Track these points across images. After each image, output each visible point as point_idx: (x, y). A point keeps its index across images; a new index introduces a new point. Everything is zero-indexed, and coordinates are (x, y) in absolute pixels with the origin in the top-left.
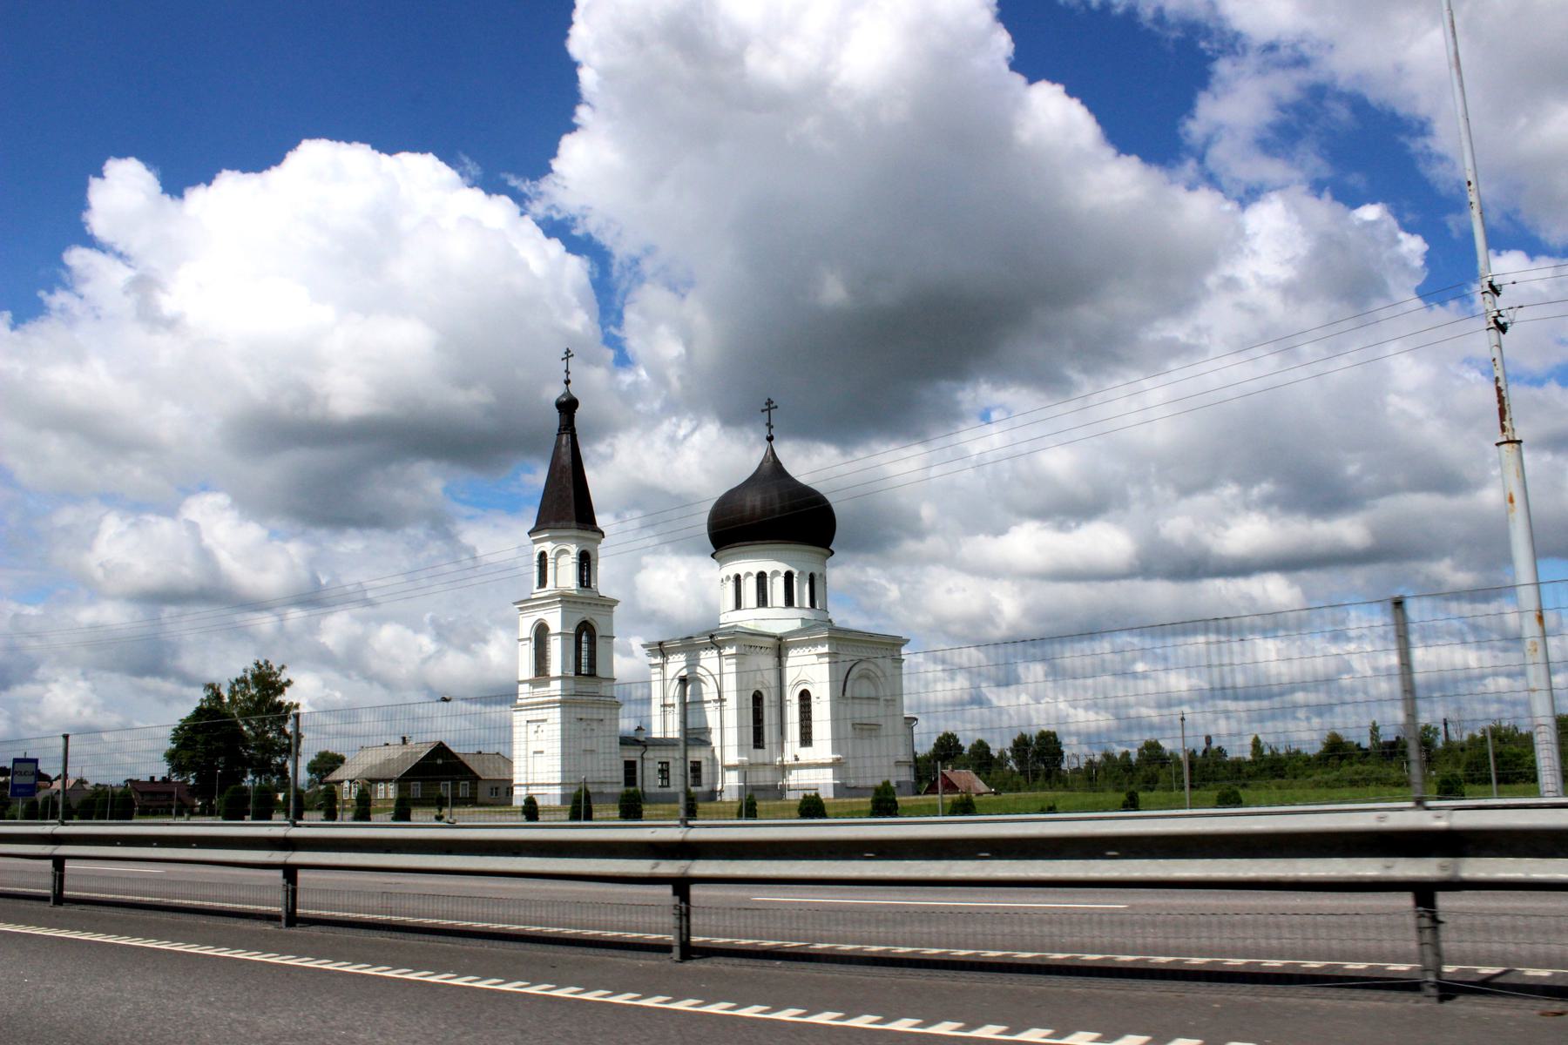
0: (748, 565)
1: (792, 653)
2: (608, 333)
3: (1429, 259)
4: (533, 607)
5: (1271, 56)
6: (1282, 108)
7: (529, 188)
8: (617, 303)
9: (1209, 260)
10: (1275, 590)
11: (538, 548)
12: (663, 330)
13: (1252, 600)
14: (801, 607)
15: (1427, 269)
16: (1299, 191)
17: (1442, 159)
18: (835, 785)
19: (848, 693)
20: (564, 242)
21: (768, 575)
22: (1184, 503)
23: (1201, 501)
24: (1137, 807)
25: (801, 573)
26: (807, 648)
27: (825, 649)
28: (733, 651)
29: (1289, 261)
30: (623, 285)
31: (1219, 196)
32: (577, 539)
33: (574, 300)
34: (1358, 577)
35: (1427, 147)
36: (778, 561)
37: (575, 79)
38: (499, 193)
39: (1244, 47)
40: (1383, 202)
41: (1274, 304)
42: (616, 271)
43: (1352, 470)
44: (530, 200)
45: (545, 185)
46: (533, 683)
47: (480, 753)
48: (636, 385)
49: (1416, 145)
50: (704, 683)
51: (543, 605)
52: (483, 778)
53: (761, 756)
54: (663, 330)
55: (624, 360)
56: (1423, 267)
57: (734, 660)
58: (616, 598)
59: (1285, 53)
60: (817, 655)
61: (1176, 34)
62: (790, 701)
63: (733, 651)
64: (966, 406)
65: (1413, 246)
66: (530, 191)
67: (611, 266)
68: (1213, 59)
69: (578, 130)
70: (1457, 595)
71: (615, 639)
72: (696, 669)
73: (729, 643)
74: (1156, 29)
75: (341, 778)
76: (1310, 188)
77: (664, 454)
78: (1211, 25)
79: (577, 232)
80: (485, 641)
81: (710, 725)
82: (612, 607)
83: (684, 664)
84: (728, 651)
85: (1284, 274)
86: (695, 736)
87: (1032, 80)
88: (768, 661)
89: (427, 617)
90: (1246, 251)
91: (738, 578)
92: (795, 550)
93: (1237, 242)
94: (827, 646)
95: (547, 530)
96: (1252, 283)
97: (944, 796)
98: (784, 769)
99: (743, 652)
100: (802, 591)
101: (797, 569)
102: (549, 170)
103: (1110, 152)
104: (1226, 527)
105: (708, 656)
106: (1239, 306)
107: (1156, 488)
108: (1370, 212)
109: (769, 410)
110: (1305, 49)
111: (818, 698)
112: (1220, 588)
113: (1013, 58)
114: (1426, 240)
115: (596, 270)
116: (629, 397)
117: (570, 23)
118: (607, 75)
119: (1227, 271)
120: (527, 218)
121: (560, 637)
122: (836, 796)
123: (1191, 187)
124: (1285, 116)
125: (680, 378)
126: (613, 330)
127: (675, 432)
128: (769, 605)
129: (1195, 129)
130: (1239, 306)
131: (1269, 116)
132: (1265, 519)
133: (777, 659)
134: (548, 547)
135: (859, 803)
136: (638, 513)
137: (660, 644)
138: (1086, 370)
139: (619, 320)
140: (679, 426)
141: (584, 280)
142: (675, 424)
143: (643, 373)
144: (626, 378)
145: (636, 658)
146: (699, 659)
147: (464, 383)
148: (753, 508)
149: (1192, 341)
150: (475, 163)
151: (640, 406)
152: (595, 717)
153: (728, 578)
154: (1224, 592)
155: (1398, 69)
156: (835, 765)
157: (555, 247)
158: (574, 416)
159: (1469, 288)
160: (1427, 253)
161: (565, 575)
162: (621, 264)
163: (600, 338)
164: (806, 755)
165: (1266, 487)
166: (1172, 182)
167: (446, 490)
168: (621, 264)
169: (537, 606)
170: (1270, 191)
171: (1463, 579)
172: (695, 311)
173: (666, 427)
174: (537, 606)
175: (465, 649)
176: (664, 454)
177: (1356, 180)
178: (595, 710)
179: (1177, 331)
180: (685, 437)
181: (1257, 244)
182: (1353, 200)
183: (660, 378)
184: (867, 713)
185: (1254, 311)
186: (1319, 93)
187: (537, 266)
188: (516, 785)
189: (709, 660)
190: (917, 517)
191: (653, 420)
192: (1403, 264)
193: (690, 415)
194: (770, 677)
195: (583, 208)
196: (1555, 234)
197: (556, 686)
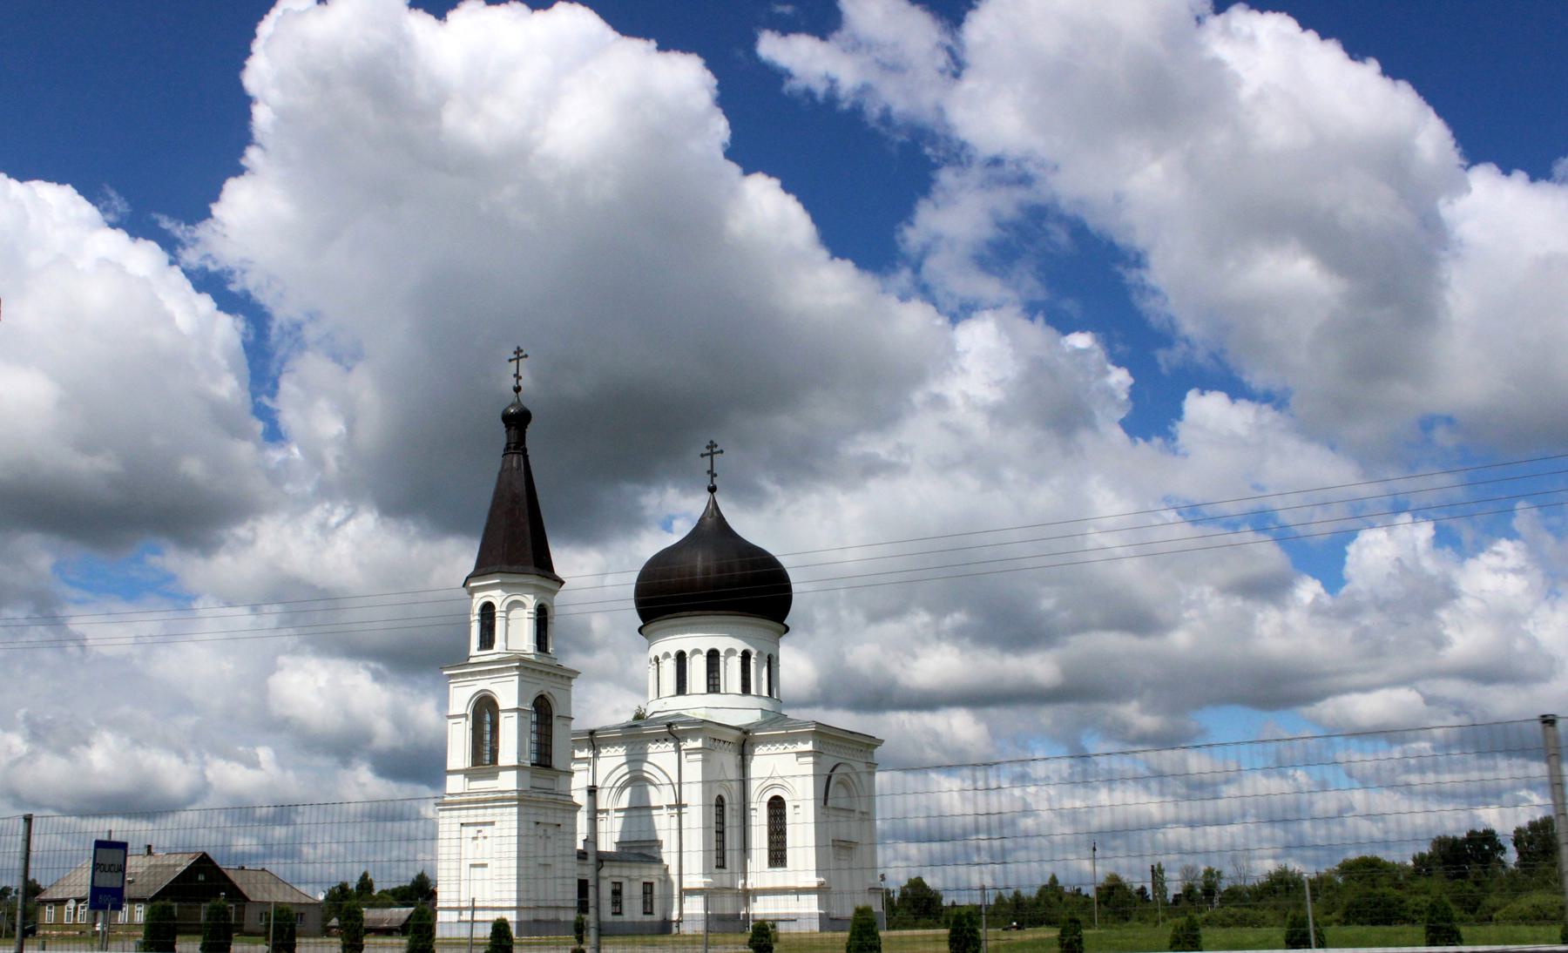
0: (695, 641)
1: (760, 750)
2: (260, 403)
3: (1134, 392)
4: (472, 674)
5: (995, 171)
6: (1000, 225)
7: (183, 232)
8: (273, 369)
9: (916, 376)
10: (961, 726)
11: (478, 600)
12: (323, 404)
13: (936, 735)
14: (759, 696)
15: (1131, 404)
16: (1012, 313)
17: (1155, 292)
18: (820, 914)
19: (830, 803)
20: (216, 298)
21: (722, 654)
22: (873, 630)
23: (891, 628)
24: (1197, 946)
25: (759, 653)
26: (782, 744)
27: (809, 746)
28: (699, 744)
29: (998, 383)
30: (281, 352)
31: (931, 309)
32: (537, 590)
33: (224, 363)
34: (1046, 716)
35: (1142, 280)
36: (735, 637)
37: (248, 115)
38: (147, 237)
39: (970, 159)
40: (1092, 332)
41: (978, 425)
42: (274, 333)
43: (1047, 604)
44: (184, 247)
45: (203, 230)
46: (469, 774)
47: (263, 870)
48: (286, 463)
49: (1131, 276)
50: (655, 785)
51: (490, 671)
52: (252, 899)
53: (724, 879)
54: (323, 404)
55: (274, 435)
56: (1127, 400)
57: (700, 756)
58: (576, 669)
59: (1009, 168)
60: (797, 753)
61: (901, 138)
62: (755, 809)
63: (699, 744)
64: (649, 512)
65: (1120, 378)
66: (184, 236)
67: (269, 328)
68: (936, 167)
69: (246, 173)
70: (1144, 739)
71: (573, 721)
72: (642, 766)
73: (693, 734)
74: (883, 129)
75: (66, 896)
76: (1024, 310)
77: (313, 543)
78: (938, 131)
79: (233, 288)
80: (87, 744)
81: (661, 836)
82: (570, 679)
83: (624, 760)
84: (690, 744)
85: (992, 396)
86: (641, 850)
87: (748, 171)
88: (730, 760)
89: (21, 714)
90: (956, 369)
91: (681, 657)
92: (731, 623)
93: (947, 359)
94: (811, 742)
95: (498, 574)
96: (959, 402)
97: (988, 930)
98: (748, 895)
99: (708, 746)
100: (759, 675)
101: (755, 648)
102: (207, 214)
103: (823, 254)
104: (915, 657)
105: (659, 750)
106: (946, 426)
107: (844, 613)
108: (1081, 340)
109: (712, 454)
110: (1030, 168)
111: (796, 807)
112: (903, 722)
113: (729, 144)
114: (1132, 373)
115: (252, 333)
116: (276, 477)
117: (248, 53)
118: (284, 117)
119: (935, 388)
120: (176, 269)
121: (515, 714)
122: (822, 929)
123: (904, 298)
124: (1006, 235)
125: (338, 459)
126: (266, 400)
127: (327, 519)
128: (722, 691)
129: (913, 237)
130: (946, 426)
131: (988, 232)
132: (956, 651)
133: (740, 757)
134: (498, 598)
135: (1535, 940)
136: (277, 608)
137: (592, 733)
138: (781, 481)
139: (273, 392)
140: (331, 512)
141: (237, 342)
142: (327, 511)
143: (296, 451)
144: (276, 455)
145: (262, 769)
146: (647, 754)
147: (86, 446)
148: (706, 571)
149: (894, 459)
150: (123, 199)
151: (288, 487)
152: (551, 820)
153: (667, 655)
154: (908, 726)
155: (1118, 198)
156: (820, 890)
157: (205, 303)
158: (525, 432)
159: (1173, 426)
160: (1132, 387)
161: (518, 633)
162: (281, 327)
163: (249, 407)
164: (777, 878)
165: (959, 618)
166: (884, 292)
167: (57, 568)
168: (281, 327)
169: (480, 673)
170: (987, 309)
171: (1149, 722)
172: (364, 387)
173: (317, 513)
174: (480, 673)
175: (63, 751)
176: (313, 543)
177: (1070, 305)
178: (549, 812)
179: (878, 446)
180: (338, 525)
181: (968, 362)
182: (1063, 325)
183: (317, 462)
184: (848, 829)
185: (959, 432)
186: (1039, 215)
187: (184, 321)
188: (442, 909)
189: (661, 757)
190: (587, 629)
191: (301, 506)
192: (1110, 394)
193: (346, 502)
194: (732, 773)
195: (243, 260)
196: (1257, 379)
197: (508, 782)
